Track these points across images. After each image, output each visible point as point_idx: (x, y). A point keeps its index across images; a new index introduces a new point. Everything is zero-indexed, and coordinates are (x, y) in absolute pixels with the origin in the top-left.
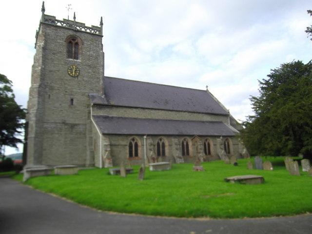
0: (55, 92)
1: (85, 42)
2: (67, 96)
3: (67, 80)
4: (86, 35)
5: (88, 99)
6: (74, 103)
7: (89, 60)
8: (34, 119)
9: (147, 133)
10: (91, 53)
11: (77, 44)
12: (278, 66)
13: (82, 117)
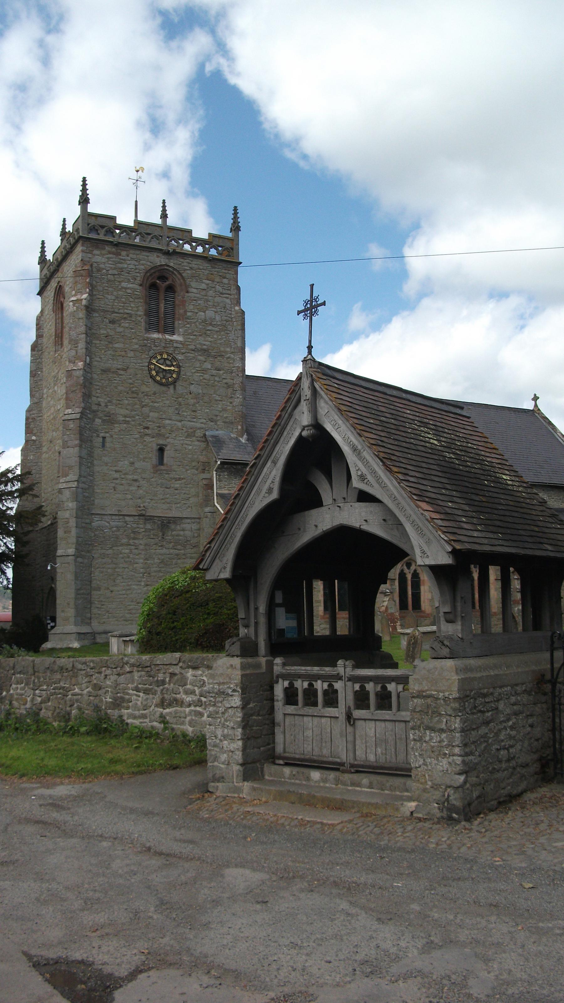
0: (117, 428)
1: (194, 284)
2: (147, 439)
4: (195, 263)
5: (203, 445)
8: (72, 505)
10: (210, 313)
11: (171, 289)
12: (78, 199)
13: (188, 499)
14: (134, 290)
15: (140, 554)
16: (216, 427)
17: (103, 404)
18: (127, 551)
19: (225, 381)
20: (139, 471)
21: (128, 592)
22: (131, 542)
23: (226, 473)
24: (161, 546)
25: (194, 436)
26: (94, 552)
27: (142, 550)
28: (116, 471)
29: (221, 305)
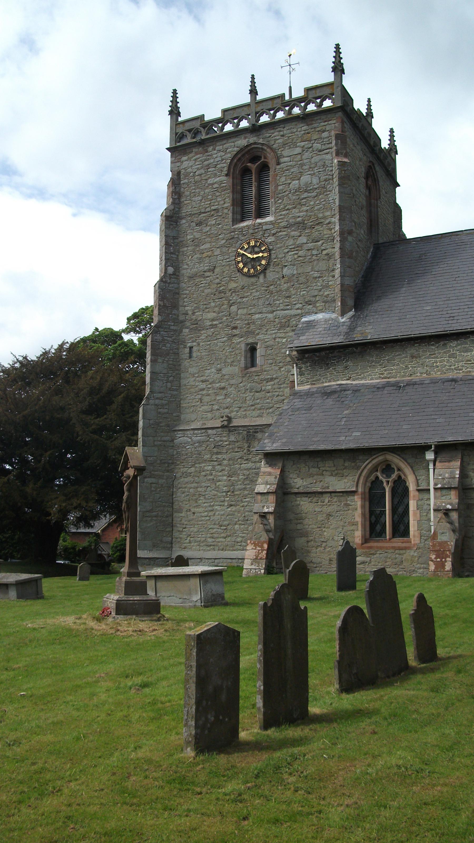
3: (234, 291)
6: (259, 360)
7: (299, 204)
9: (433, 440)
10: (305, 179)
14: (221, 182)
15: (223, 470)
16: (315, 309)
17: (190, 313)
18: (210, 468)
19: (324, 252)
20: (226, 377)
21: (211, 513)
22: (214, 457)
23: (308, 364)
24: (247, 460)
25: (288, 326)
26: (176, 471)
27: (226, 466)
28: (203, 381)
29: (319, 164)
